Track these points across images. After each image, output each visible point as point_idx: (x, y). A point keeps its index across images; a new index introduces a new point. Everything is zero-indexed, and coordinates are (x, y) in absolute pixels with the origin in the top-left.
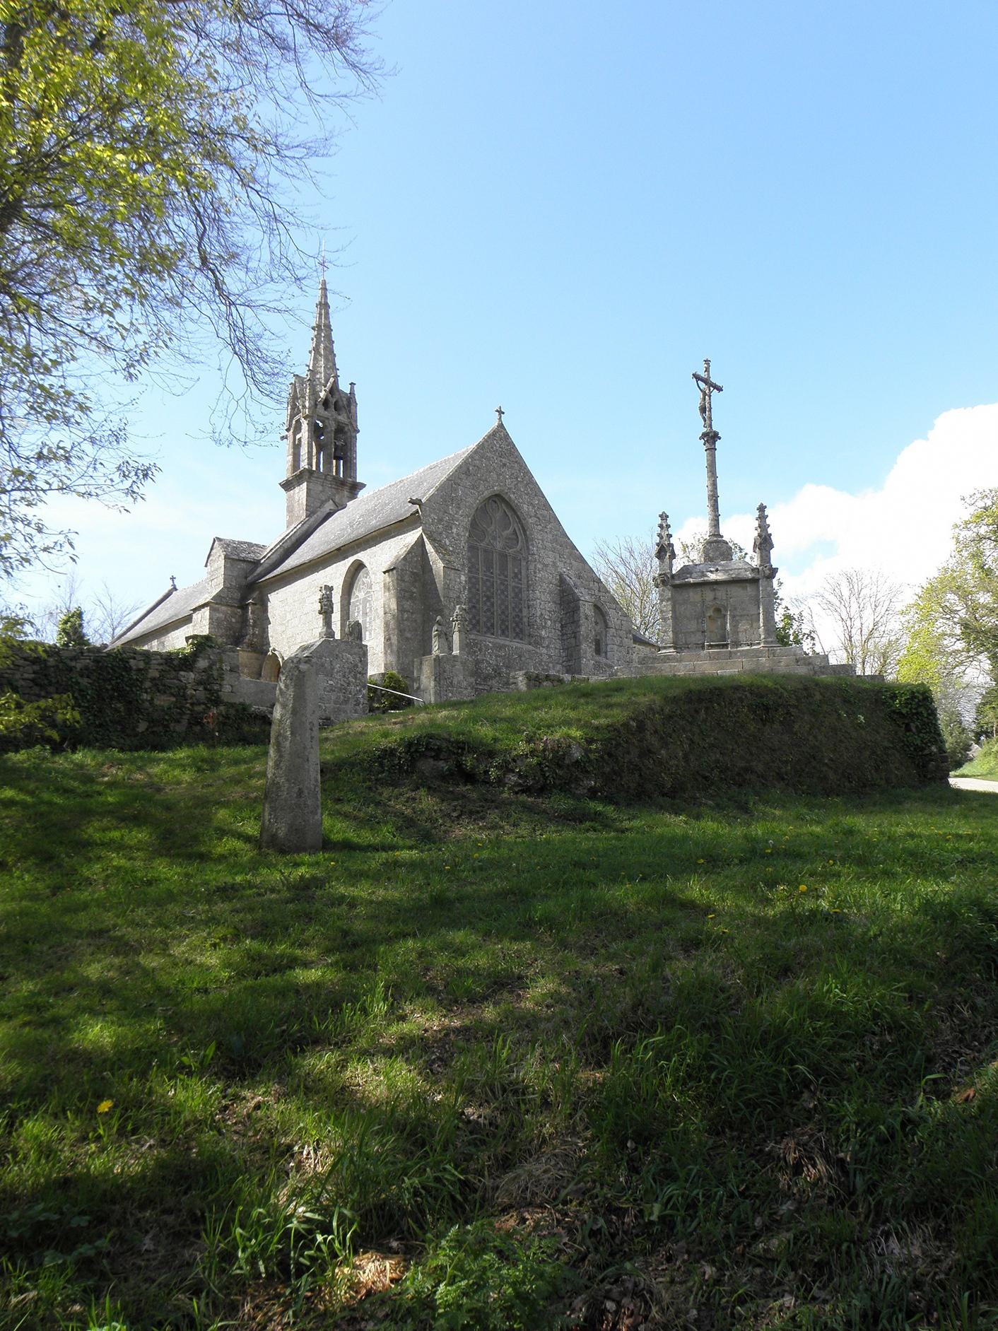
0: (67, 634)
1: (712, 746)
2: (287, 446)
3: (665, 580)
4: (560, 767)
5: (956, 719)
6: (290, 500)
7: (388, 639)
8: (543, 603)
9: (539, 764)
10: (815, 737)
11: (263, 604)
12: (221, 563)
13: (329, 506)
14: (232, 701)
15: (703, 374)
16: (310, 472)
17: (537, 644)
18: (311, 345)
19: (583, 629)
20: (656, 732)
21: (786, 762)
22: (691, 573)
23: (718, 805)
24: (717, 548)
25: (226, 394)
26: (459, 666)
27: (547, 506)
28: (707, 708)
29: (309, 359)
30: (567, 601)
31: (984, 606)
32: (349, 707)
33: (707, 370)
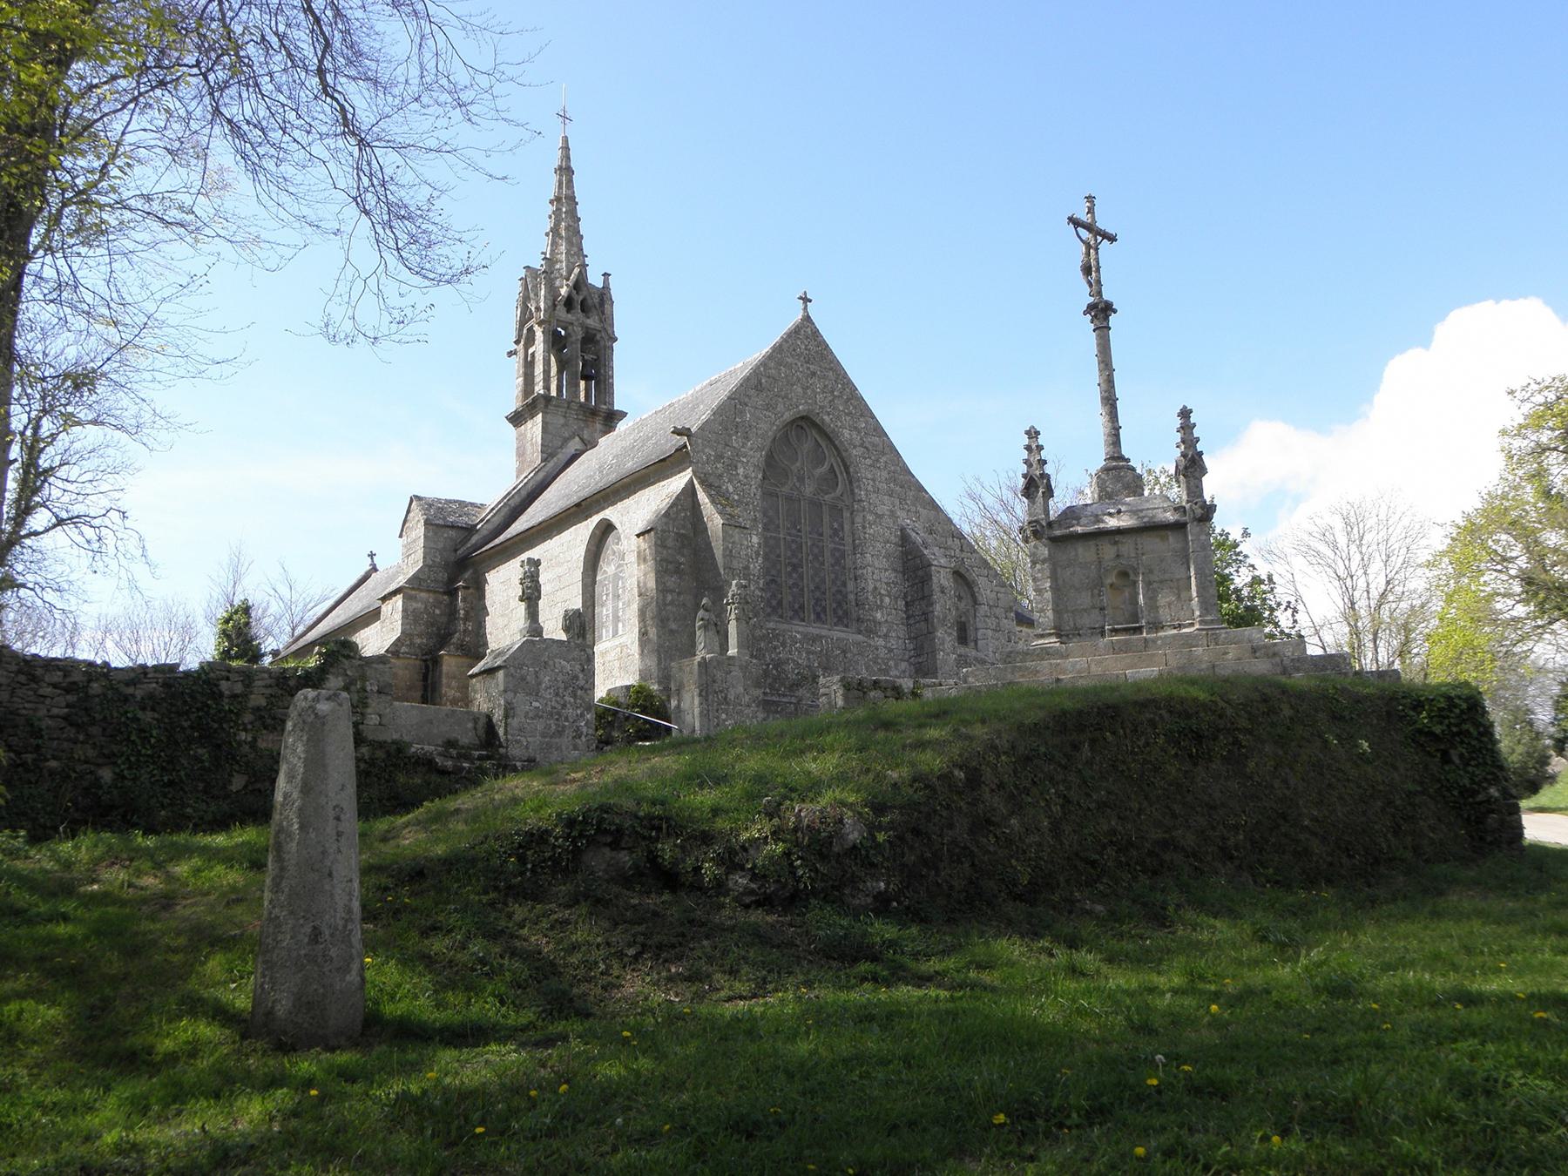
0: (228, 637)
1: (1102, 805)
2: (516, 363)
3: (1039, 530)
4: (823, 857)
5: (1523, 717)
6: (521, 438)
7: (643, 634)
8: (877, 572)
9: (787, 854)
10: (1285, 781)
11: (479, 586)
12: (420, 531)
13: (575, 444)
14: (381, 738)
15: (1086, 218)
16: (547, 398)
17: (870, 632)
18: (548, 225)
19: (938, 607)
20: (1001, 786)
21: (1236, 827)
22: (1078, 519)
23: (1112, 913)
24: (1118, 475)
25: (350, 270)
26: (736, 673)
27: (879, 431)
28: (1093, 741)
29: (544, 244)
30: (913, 568)
31: (1556, 550)
32: (565, 741)
33: (1091, 211)
